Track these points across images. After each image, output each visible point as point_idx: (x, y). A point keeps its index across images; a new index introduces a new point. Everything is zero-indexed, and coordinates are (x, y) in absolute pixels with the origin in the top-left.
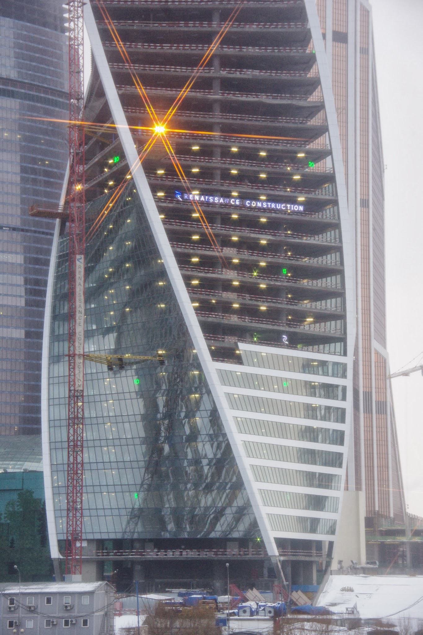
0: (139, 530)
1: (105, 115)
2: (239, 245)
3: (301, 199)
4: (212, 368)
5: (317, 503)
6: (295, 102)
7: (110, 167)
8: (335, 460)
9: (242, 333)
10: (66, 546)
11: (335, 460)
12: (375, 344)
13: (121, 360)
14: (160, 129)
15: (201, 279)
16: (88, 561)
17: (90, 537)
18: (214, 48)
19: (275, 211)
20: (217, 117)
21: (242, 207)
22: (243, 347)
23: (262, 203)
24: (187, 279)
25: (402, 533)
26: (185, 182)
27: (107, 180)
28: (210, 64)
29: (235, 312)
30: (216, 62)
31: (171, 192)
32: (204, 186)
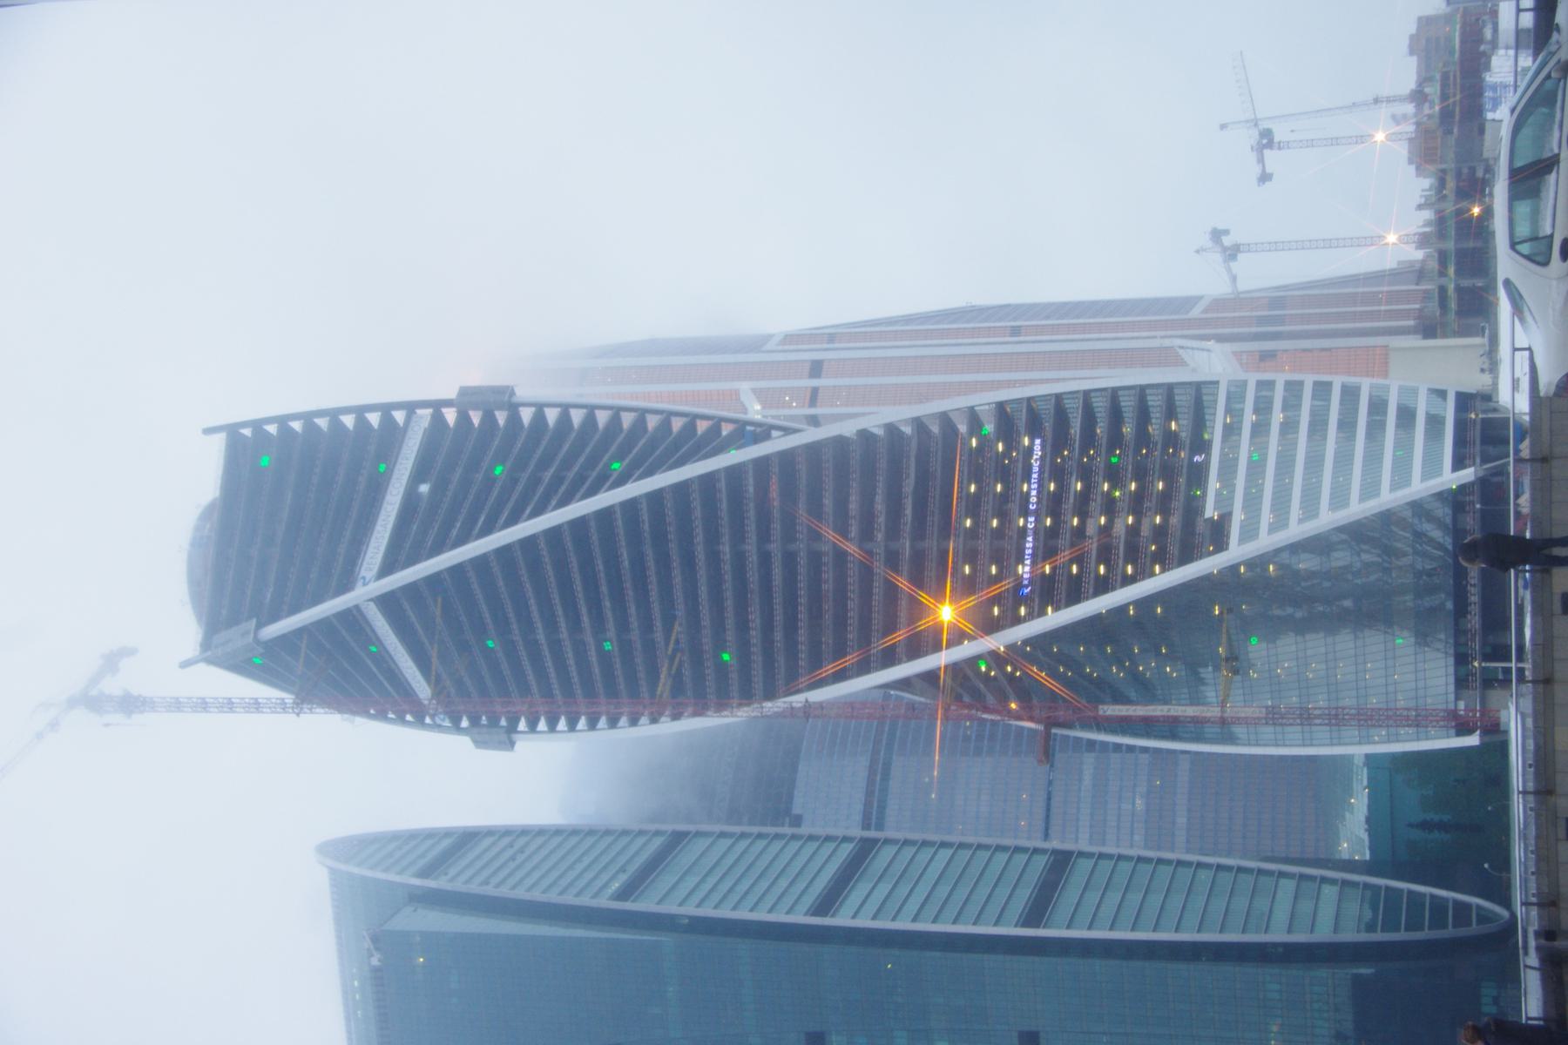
0: (1443, 637)
1: (930, 677)
2: (1083, 515)
3: (1026, 441)
4: (1237, 551)
5: (1406, 416)
6: (913, 453)
7: (989, 669)
8: (1350, 393)
9: (1193, 509)
10: (1463, 729)
11: (1350, 393)
12: (1196, 312)
13: (1227, 660)
14: (947, 613)
15: (1126, 562)
16: (1483, 701)
17: (1452, 697)
18: (851, 548)
19: (1041, 472)
20: (931, 544)
21: (1037, 513)
22: (1211, 512)
23: (1031, 488)
24: (1128, 581)
25: (1442, 290)
26: (1007, 584)
27: (1005, 673)
28: (870, 553)
29: (1165, 520)
30: (869, 546)
31: (1019, 599)
32: (1013, 560)
